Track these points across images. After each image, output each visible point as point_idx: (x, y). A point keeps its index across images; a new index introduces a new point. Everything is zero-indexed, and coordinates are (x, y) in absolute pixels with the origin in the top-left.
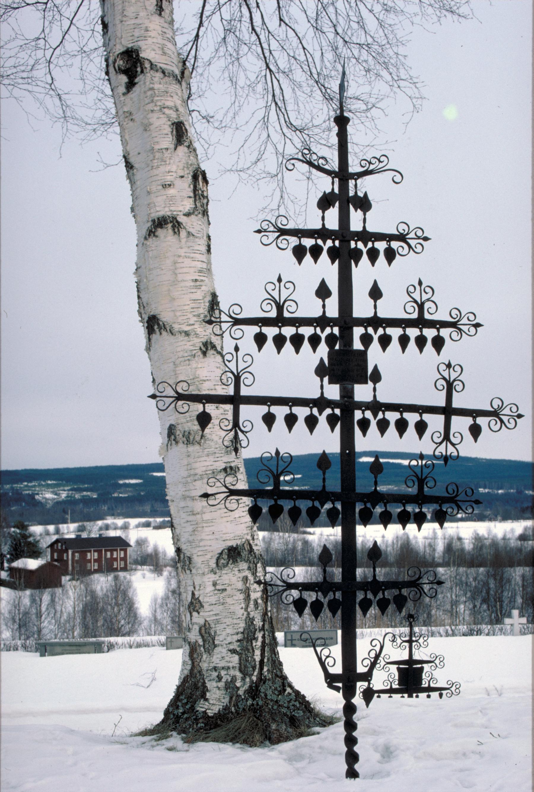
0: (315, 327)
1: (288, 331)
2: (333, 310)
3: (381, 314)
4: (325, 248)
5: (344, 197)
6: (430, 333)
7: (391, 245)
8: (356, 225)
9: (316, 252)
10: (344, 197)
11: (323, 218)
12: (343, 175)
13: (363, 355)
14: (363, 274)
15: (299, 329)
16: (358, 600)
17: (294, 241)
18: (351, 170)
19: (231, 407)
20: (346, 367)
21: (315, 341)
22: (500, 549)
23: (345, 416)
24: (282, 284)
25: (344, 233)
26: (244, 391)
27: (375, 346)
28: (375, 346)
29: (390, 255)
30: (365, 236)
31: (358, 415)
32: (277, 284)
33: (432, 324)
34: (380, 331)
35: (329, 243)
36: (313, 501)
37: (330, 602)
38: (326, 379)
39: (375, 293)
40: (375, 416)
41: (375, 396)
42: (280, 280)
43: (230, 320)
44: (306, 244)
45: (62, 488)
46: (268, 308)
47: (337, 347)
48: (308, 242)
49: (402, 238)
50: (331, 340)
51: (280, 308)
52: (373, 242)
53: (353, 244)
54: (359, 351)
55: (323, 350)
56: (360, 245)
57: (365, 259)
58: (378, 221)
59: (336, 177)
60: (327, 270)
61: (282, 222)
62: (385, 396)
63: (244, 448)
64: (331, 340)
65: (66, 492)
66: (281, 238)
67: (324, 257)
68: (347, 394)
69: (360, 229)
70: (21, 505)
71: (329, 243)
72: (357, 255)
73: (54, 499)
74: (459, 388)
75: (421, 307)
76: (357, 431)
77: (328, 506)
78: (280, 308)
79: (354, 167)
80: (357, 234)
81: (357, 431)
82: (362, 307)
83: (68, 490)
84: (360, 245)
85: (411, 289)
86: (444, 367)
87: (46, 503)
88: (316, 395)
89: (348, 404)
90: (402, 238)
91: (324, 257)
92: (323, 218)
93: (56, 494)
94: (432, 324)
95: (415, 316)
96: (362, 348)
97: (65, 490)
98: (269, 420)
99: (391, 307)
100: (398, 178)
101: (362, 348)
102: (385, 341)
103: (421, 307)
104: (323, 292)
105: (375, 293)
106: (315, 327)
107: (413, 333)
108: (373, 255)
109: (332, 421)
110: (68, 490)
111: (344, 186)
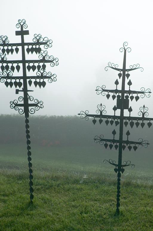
0: (114, 93)
3: (129, 140)
12: (124, 70)
24: (102, 106)
30: (127, 142)
31: (124, 121)
34: (129, 145)
37: (115, 146)
41: (130, 89)
43: (143, 144)
46: (98, 112)
48: (109, 143)
49: (140, 143)
51: (101, 112)
52: (132, 120)
53: (123, 144)
59: (117, 166)
62: (133, 88)
64: (118, 96)
66: (99, 111)
69: (128, 90)
76: (124, 125)
77: (115, 144)
78: (101, 112)
79: (127, 68)
81: (124, 125)
84: (125, 145)
86: (149, 91)
88: (115, 89)
90: (140, 143)
95: (141, 116)
104: (114, 133)
105: (128, 133)
106: (114, 93)
109: (117, 123)
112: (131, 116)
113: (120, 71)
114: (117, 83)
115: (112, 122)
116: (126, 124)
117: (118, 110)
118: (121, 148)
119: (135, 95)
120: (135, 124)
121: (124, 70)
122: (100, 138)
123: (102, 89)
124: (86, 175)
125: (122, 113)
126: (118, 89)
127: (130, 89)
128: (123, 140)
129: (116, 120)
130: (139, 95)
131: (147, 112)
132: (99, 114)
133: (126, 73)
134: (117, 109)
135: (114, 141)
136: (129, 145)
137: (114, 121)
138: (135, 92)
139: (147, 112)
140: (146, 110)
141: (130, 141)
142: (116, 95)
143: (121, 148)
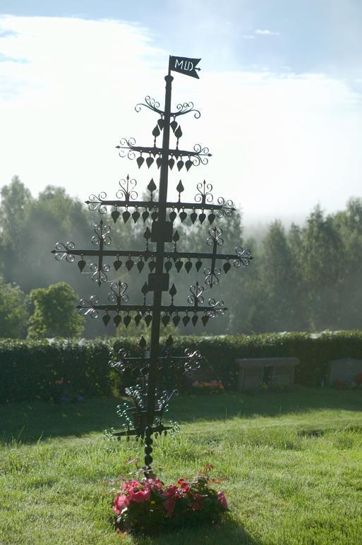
2: (160, 145)
3: (180, 149)
4: (155, 159)
5: (167, 123)
6: (200, 314)
7: (188, 159)
8: (172, 146)
9: (150, 161)
10: (167, 123)
11: (155, 141)
12: (167, 113)
13: (167, 276)
14: (174, 175)
16: (164, 262)
17: (138, 154)
19: (98, 257)
20: (158, 283)
21: (145, 216)
22: (245, 236)
23: (158, 315)
24: (129, 180)
25: (165, 150)
27: (174, 269)
28: (174, 269)
29: (189, 164)
30: (178, 153)
31: (166, 260)
32: (126, 180)
35: (157, 156)
36: (150, 153)
38: (150, 239)
39: (180, 188)
40: (175, 260)
44: (144, 155)
48: (146, 156)
50: (151, 265)
51: (127, 195)
53: (170, 157)
54: (168, 222)
55: (150, 221)
56: (174, 158)
57: (175, 166)
58: (185, 144)
60: (154, 173)
61: (132, 141)
67: (154, 164)
68: (161, 247)
69: (175, 149)
71: (157, 156)
75: (204, 197)
78: (127, 195)
79: (173, 110)
80: (172, 151)
82: (172, 196)
85: (200, 186)
89: (157, 307)
91: (154, 164)
92: (155, 141)
96: (170, 220)
98: (117, 265)
99: (189, 197)
100: (197, 116)
101: (170, 220)
102: (179, 266)
103: (204, 197)
104: (151, 186)
105: (180, 188)
107: (191, 314)
108: (180, 165)
109: (148, 320)
111: (158, 283)
112: (182, 201)
114: (156, 133)
116: (166, 320)
117: (150, 292)
118: (165, 165)
119: (185, 159)
120: (181, 319)
121: (167, 113)
125: (158, 298)
128: (162, 304)
129: (147, 313)
130: (192, 158)
133: (172, 119)
137: (155, 159)
138: (185, 153)
143: (165, 165)
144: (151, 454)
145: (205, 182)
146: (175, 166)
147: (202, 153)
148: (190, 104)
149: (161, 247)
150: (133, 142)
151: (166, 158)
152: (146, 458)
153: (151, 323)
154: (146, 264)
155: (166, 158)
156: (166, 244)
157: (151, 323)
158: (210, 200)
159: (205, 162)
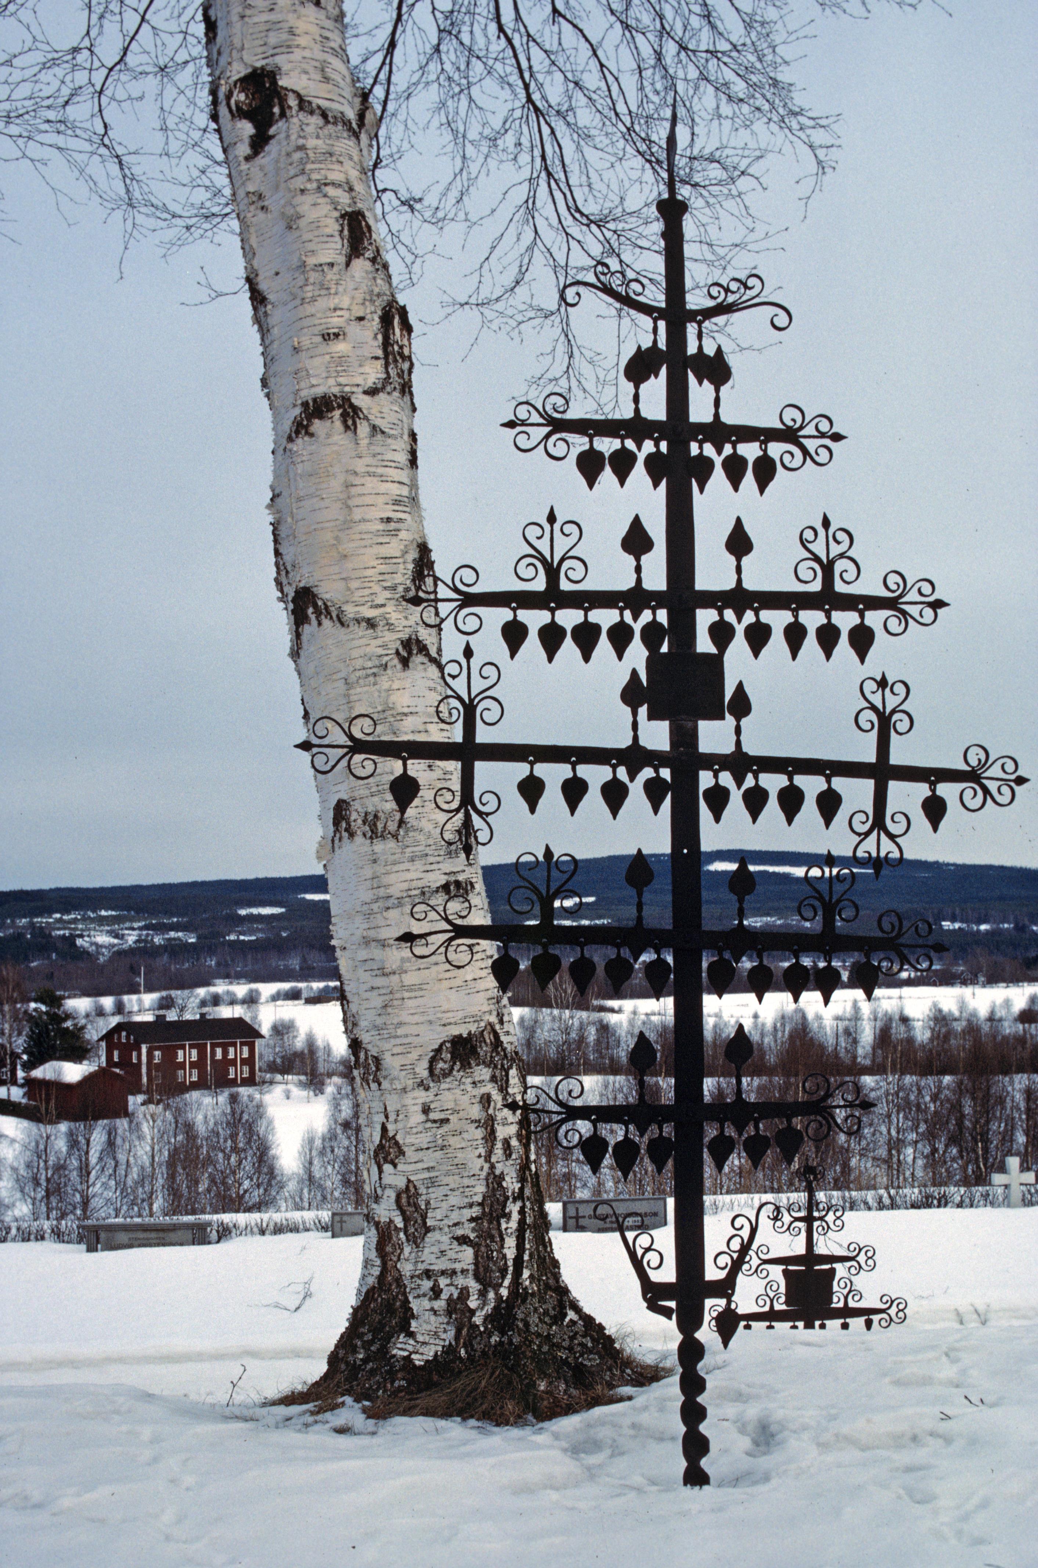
1: (569, 618)
2: (656, 578)
3: (729, 417)
4: (641, 457)
7: (761, 453)
10: (675, 359)
12: (676, 314)
14: (716, 505)
15: (590, 613)
17: (580, 443)
18: (480, 767)
20: (682, 686)
21: (620, 637)
24: (557, 527)
25: (677, 425)
26: (483, 735)
29: (765, 471)
30: (718, 432)
31: (706, 780)
33: (850, 602)
34: (749, 617)
35: (648, 446)
38: (643, 711)
39: (739, 543)
40: (739, 783)
41: (738, 743)
42: (552, 518)
43: (456, 596)
45: (127, 925)
46: (529, 573)
47: (664, 649)
48: (607, 445)
51: (552, 573)
54: (706, 656)
55: (637, 654)
56: (709, 450)
57: (718, 476)
63: (484, 844)
65: (136, 933)
68: (685, 738)
69: (708, 418)
70: (49, 957)
71: (648, 446)
72: (702, 470)
73: (114, 946)
74: (903, 726)
78: (552, 573)
79: (695, 300)
80: (701, 428)
82: (713, 571)
83: (141, 929)
87: (98, 953)
93: (117, 936)
94: (850, 602)
96: (713, 650)
97: (133, 929)
100: (782, 320)
101: (713, 650)
103: (828, 569)
104: (636, 541)
105: (739, 543)
109: (655, 792)
110: (141, 929)
113: (655, 315)
115: (622, 464)
116: (718, 799)
118: (680, 475)
119: (750, 451)
122: (562, 560)
123: (456, 590)
124: (542, 1388)
125: (677, 398)
126: (647, 585)
127: (738, 743)
131: (910, 620)
132: (540, 584)
134: (646, 653)
135: (637, 427)
136: (749, 617)
139: (910, 620)
140: (916, 616)
141: (751, 753)
142: (643, 1142)
143: (680, 475)
144: (698, 1335)
145: (826, 523)
146: (718, 476)
147: (913, 596)
148: (752, 282)
149: (685, 738)
150: (468, 576)
151: (679, 457)
152: (682, 1348)
153: (670, 1163)
154: (636, 789)
155: (679, 457)
156: (703, 726)
157: (670, 1163)
158: (850, 576)
159: (1005, 799)
